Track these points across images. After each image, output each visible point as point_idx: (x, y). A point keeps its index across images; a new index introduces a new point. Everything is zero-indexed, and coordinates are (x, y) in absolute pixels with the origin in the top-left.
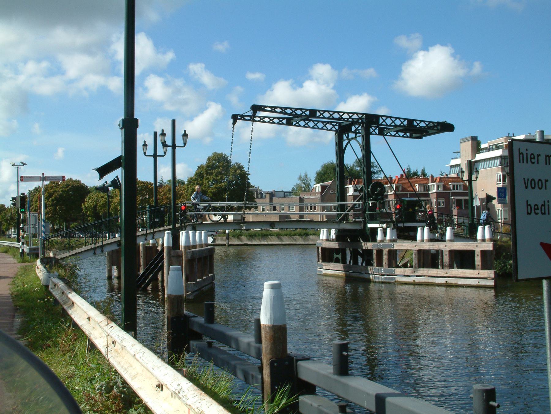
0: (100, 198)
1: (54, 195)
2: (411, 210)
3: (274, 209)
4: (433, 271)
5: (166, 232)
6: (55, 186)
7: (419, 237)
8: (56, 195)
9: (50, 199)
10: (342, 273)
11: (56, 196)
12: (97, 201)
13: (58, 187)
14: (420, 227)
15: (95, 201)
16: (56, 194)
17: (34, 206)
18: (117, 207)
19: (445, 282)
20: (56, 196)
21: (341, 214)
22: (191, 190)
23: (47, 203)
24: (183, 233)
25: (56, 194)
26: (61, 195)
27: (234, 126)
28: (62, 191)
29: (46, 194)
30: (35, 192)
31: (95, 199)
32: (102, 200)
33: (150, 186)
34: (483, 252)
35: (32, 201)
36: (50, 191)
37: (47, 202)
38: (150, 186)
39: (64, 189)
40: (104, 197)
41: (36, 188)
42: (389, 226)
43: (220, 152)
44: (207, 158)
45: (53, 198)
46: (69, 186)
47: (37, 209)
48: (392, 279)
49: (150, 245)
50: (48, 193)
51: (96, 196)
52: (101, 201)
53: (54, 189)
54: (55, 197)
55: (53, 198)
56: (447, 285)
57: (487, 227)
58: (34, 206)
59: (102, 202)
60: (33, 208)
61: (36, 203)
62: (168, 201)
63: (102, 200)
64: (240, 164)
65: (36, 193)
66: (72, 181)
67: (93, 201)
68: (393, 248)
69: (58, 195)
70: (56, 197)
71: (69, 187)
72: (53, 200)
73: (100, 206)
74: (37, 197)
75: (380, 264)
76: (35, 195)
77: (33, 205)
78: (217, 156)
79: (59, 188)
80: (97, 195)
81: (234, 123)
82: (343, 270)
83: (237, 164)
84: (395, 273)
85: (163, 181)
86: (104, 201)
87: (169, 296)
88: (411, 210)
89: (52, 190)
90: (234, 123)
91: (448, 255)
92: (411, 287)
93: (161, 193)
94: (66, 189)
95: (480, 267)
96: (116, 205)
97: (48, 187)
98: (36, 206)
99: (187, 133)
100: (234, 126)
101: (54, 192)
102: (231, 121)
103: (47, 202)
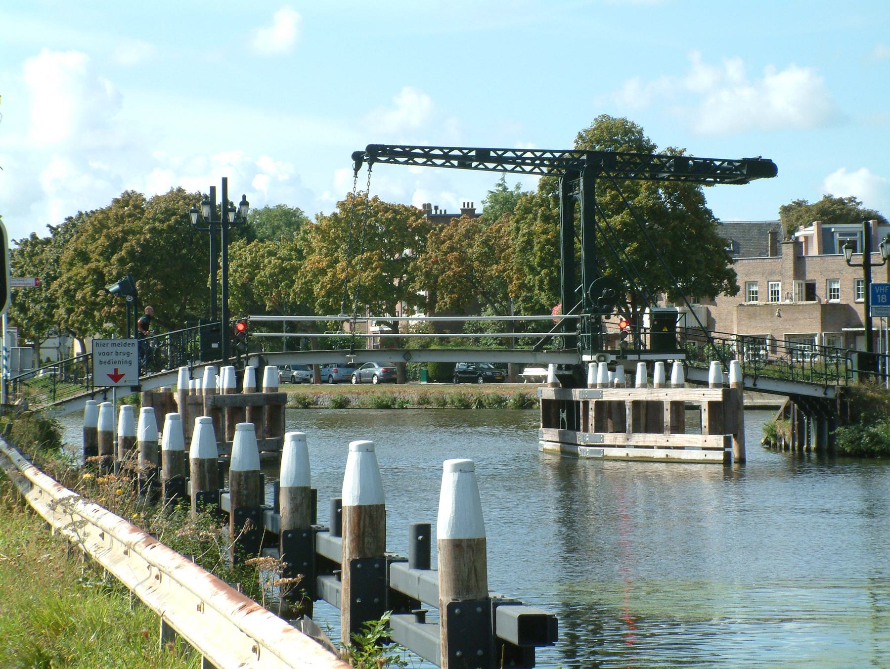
0: (263, 256)
1: (125, 245)
2: (665, 330)
3: (810, 292)
4: (651, 438)
5: (207, 367)
6: (130, 216)
7: (590, 381)
8: (134, 243)
9: (115, 257)
10: (557, 447)
11: (132, 246)
12: (255, 266)
13: (140, 219)
14: (658, 361)
15: (249, 265)
16: (132, 241)
17: (64, 278)
18: (312, 286)
19: (665, 457)
20: (132, 246)
21: (539, 339)
22: (524, 235)
23: (105, 270)
24: (224, 369)
25: (132, 241)
26: (145, 246)
27: (356, 174)
28: (153, 230)
29: (102, 240)
30: (66, 232)
31: (249, 260)
32: (270, 262)
33: (412, 218)
34: (712, 404)
35: (57, 261)
36: (113, 230)
37: (106, 266)
38: (412, 218)
39: (157, 224)
40: (275, 255)
41: (70, 219)
42: (603, 358)
43: (616, 114)
44: (575, 136)
45: (123, 253)
46: (174, 214)
47: (72, 287)
48: (599, 452)
49: (264, 392)
50: (108, 237)
51: (251, 252)
52: (265, 266)
53: (127, 225)
54: (128, 253)
55: (123, 253)
56: (668, 461)
57: (600, 364)
58: (64, 278)
59: (268, 271)
60: (60, 287)
61: (69, 270)
62: (463, 270)
63: (270, 262)
64: (681, 152)
65: (72, 236)
66: (185, 198)
67: (241, 266)
68: (602, 397)
69: (138, 243)
70: (131, 253)
71: (173, 219)
72: (122, 261)
73: (261, 283)
74: (72, 248)
75: (586, 430)
76: (67, 241)
77: (61, 274)
78: (607, 128)
79: (144, 219)
80: (255, 246)
81: (357, 168)
82: (557, 440)
83: (672, 150)
84: (603, 442)
85: (505, 189)
86: (275, 267)
87: (200, 463)
88: (665, 330)
89: (120, 229)
90: (357, 168)
91: (669, 410)
92: (624, 464)
93: (444, 242)
94: (165, 226)
95: (707, 430)
96: (310, 281)
97: (108, 218)
98: (70, 279)
99: (247, 200)
100: (356, 174)
101: (126, 233)
102: (352, 163)
103: (106, 266)
